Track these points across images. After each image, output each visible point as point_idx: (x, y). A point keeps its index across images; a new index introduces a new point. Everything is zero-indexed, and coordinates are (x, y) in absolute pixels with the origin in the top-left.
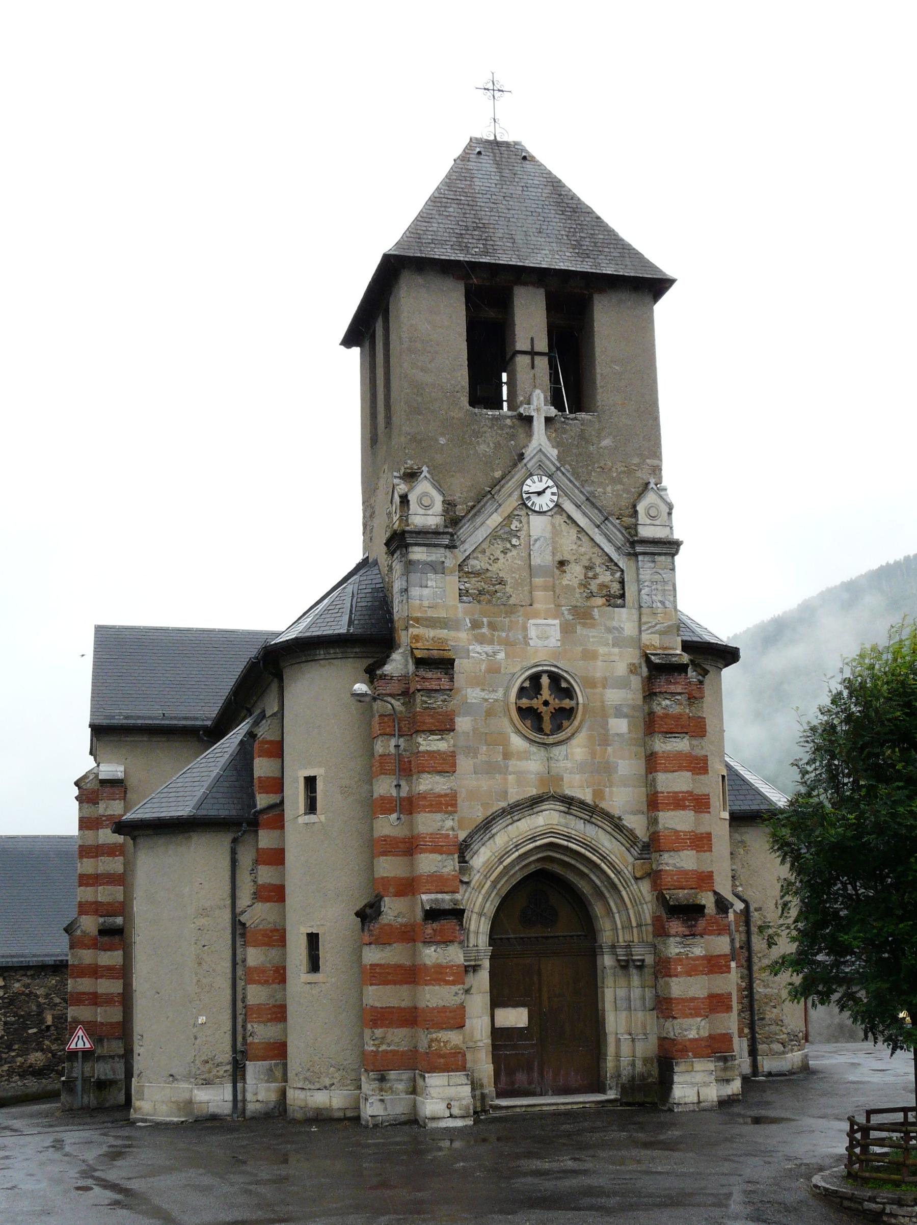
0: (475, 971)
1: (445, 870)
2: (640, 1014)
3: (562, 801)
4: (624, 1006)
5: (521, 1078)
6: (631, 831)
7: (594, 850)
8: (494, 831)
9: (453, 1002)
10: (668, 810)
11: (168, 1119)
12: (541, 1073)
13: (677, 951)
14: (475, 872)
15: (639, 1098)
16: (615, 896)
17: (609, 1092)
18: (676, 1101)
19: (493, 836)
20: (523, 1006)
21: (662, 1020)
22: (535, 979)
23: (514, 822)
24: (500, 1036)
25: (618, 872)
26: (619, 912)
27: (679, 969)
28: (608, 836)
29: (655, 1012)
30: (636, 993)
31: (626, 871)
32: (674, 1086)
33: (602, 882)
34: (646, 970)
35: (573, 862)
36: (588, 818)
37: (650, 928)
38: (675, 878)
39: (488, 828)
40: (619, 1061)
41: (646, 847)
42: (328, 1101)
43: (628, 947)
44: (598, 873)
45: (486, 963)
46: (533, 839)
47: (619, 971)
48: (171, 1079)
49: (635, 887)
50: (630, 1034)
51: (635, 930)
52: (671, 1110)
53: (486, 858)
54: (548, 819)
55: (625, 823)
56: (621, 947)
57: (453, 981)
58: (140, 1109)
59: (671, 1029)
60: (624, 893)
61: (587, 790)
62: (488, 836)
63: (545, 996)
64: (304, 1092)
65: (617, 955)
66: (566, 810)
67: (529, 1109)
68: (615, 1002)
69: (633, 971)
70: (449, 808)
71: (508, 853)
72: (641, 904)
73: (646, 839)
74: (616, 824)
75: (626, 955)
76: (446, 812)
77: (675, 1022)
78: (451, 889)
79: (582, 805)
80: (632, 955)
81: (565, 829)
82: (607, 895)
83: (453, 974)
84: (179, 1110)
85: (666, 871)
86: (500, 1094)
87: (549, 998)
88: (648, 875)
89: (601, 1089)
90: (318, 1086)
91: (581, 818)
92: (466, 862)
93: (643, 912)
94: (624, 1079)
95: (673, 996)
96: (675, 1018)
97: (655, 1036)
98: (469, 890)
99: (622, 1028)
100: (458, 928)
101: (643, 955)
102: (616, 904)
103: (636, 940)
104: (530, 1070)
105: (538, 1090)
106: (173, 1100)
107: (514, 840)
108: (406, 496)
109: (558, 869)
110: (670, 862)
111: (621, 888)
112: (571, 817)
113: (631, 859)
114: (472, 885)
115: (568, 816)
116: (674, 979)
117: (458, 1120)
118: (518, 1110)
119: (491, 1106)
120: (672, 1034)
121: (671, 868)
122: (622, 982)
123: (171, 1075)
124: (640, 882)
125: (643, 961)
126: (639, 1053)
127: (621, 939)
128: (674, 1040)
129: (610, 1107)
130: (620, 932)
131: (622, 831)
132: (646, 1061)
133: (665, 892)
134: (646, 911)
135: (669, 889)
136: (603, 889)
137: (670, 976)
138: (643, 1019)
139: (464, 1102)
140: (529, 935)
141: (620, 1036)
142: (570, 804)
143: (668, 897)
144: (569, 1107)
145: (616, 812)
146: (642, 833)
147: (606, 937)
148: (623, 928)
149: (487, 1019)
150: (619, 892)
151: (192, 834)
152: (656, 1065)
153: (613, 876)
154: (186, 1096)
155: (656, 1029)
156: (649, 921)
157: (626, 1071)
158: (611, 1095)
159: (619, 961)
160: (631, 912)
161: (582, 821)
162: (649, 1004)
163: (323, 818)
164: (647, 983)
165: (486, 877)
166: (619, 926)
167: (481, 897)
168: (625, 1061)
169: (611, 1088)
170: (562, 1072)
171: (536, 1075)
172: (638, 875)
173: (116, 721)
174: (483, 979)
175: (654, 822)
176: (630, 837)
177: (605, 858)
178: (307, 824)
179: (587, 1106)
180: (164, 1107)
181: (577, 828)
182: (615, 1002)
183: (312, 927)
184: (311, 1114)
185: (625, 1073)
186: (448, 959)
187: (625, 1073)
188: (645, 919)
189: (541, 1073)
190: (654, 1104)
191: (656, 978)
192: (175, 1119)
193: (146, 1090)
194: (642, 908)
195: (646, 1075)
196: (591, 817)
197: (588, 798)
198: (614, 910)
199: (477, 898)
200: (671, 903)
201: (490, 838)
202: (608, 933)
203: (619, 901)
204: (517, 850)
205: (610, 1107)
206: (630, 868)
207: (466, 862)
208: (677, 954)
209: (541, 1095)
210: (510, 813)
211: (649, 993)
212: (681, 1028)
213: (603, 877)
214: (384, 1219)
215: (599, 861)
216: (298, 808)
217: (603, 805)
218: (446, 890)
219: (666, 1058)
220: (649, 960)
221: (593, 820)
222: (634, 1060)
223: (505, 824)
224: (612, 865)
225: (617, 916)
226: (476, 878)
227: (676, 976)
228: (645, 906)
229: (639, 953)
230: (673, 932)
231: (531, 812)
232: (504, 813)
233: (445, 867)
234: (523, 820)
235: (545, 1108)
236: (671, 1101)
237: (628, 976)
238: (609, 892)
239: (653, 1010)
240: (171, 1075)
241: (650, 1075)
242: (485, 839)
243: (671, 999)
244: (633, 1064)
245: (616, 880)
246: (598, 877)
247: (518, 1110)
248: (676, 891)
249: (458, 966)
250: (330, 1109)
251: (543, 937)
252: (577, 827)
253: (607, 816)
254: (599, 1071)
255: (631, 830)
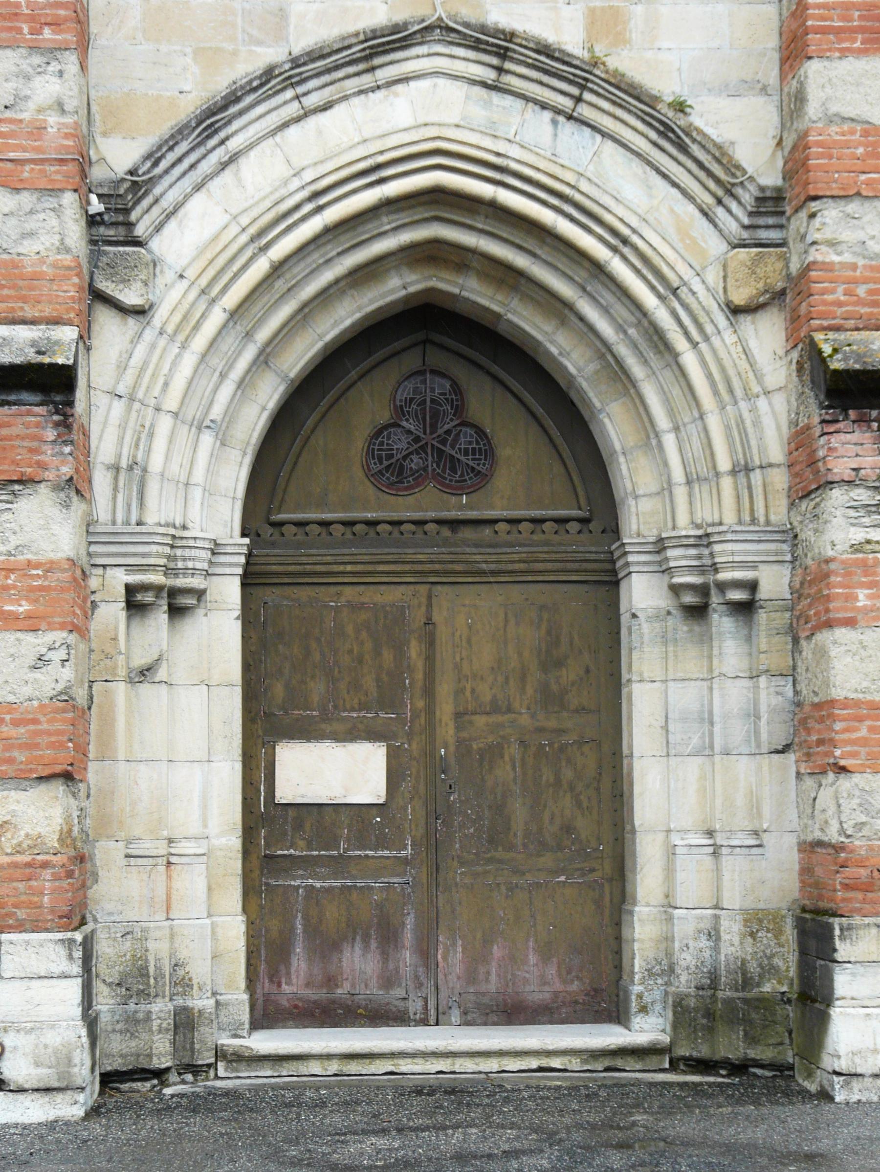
0: (176, 611)
1: (29, 247)
2: (744, 769)
3: (476, 45)
4: (695, 740)
5: (359, 966)
6: (721, 154)
7: (588, 215)
8: (234, 144)
9: (27, 691)
10: (844, 53)
12: (426, 953)
13: (858, 535)
14: (170, 276)
15: (731, 1045)
16: (667, 376)
17: (638, 1021)
18: (843, 1065)
19: (233, 158)
20: (372, 736)
21: (809, 782)
22: (414, 651)
23: (307, 114)
24: (274, 833)
25: (671, 291)
26: (676, 429)
27: (863, 598)
28: (637, 166)
29: (791, 758)
30: (732, 696)
31: (697, 286)
32: (836, 1012)
33: (621, 329)
34: (762, 616)
35: (520, 261)
36: (566, 103)
37: (780, 479)
38: (861, 291)
39: (212, 131)
40: (670, 919)
41: (771, 205)
43: (704, 540)
44: (607, 297)
45: (228, 591)
46: (374, 172)
47: (679, 626)
49: (729, 337)
50: (710, 833)
51: (727, 483)
52: (825, 1096)
53: (208, 233)
54: (430, 107)
55: (697, 120)
56: (682, 543)
57: (29, 617)
59: (832, 810)
60: (689, 360)
61: (567, 12)
62: (214, 158)
63: (445, 710)
65: (668, 571)
66: (490, 75)
67: (354, 1067)
68: (666, 728)
69: (722, 623)
70: (47, 33)
71: (286, 218)
72: (749, 396)
73: (771, 179)
74: (669, 130)
75: (701, 570)
76: (34, 48)
77: (845, 783)
78: (48, 311)
79: (548, 59)
80: (715, 568)
81: (488, 143)
82: (637, 370)
83: (32, 593)
85: (828, 267)
86: (265, 1016)
87: (458, 715)
88: (775, 298)
89: (616, 1012)
91: (544, 106)
92: (137, 243)
93: (757, 423)
94: (684, 982)
95: (838, 693)
96: (843, 769)
97: (791, 840)
98: (149, 335)
99: (686, 814)
100: (51, 434)
101: (753, 566)
102: (667, 401)
103: (730, 518)
104: (388, 936)
105: (415, 1006)
107: (308, 176)
109: (475, 292)
110: (847, 235)
111: (680, 343)
112: (508, 100)
113: (716, 246)
114: (159, 317)
115: (496, 98)
116: (841, 633)
117: (25, 1100)
118: (315, 1067)
119: (220, 1054)
120: (834, 826)
121: (847, 258)
122: (690, 661)
124: (746, 323)
125: (752, 586)
126: (733, 898)
127: (683, 519)
128: (838, 848)
129: (633, 1072)
130: (681, 493)
131: (683, 148)
132: (756, 922)
133: (819, 337)
134: (768, 422)
135: (837, 329)
136: (623, 351)
137: (829, 624)
138: (757, 785)
139: (54, 1039)
140: (395, 516)
141: (676, 839)
142: (503, 54)
143: (827, 349)
144: (492, 1065)
145: (665, 85)
146: (761, 165)
147: (640, 518)
148: (689, 482)
149: (227, 775)
150: (676, 355)
152: (790, 933)
153: (649, 300)
155: (792, 814)
156: (776, 452)
157: (690, 958)
158: (647, 1029)
159: (676, 590)
160: (714, 423)
161: (547, 115)
162: (773, 731)
164: (765, 661)
165: (208, 295)
166: (678, 475)
167: (189, 361)
168: (686, 924)
169: (644, 1009)
170: (497, 951)
171: (407, 957)
172: (739, 297)
174: (218, 634)
175: (794, 104)
176: (720, 175)
177: (625, 241)
179: (556, 1063)
181: (527, 137)
182: (666, 728)
185: (686, 959)
186: (14, 541)
187: (686, 959)
188: (762, 449)
189: (426, 953)
190: (782, 1069)
191: (796, 641)
194: (753, 410)
195: (753, 967)
196: (579, 100)
197: (570, 38)
198: (663, 422)
199: (174, 364)
200: (836, 364)
201: (224, 166)
202: (645, 505)
203: (676, 392)
204: (320, 209)
205: (633, 1072)
206: (713, 276)
207: (137, 243)
208: (856, 548)
209: (424, 1022)
210: (290, 82)
211: (772, 696)
212: (864, 807)
213: (622, 312)
215: (600, 252)
217: (624, 62)
218: (30, 312)
219: (817, 912)
220: (774, 583)
221: (584, 111)
222: (717, 917)
223: (274, 120)
224: (648, 267)
225: (669, 441)
226: (170, 299)
227: (850, 623)
228: (762, 404)
229: (735, 559)
230: (841, 468)
231: (366, 80)
232: (267, 82)
233: (31, 234)
234: (339, 110)
235: (405, 1066)
236: (828, 1062)
237: (706, 639)
238: (645, 362)
239: (784, 750)
241: (769, 970)
242: (206, 167)
243: (832, 703)
244: (714, 935)
245: (662, 317)
246: (606, 310)
247: (315, 1067)
248: (865, 334)
249: (50, 567)
251: (439, 522)
252: (526, 135)
253: (631, 96)
254: (618, 952)
255: (719, 147)
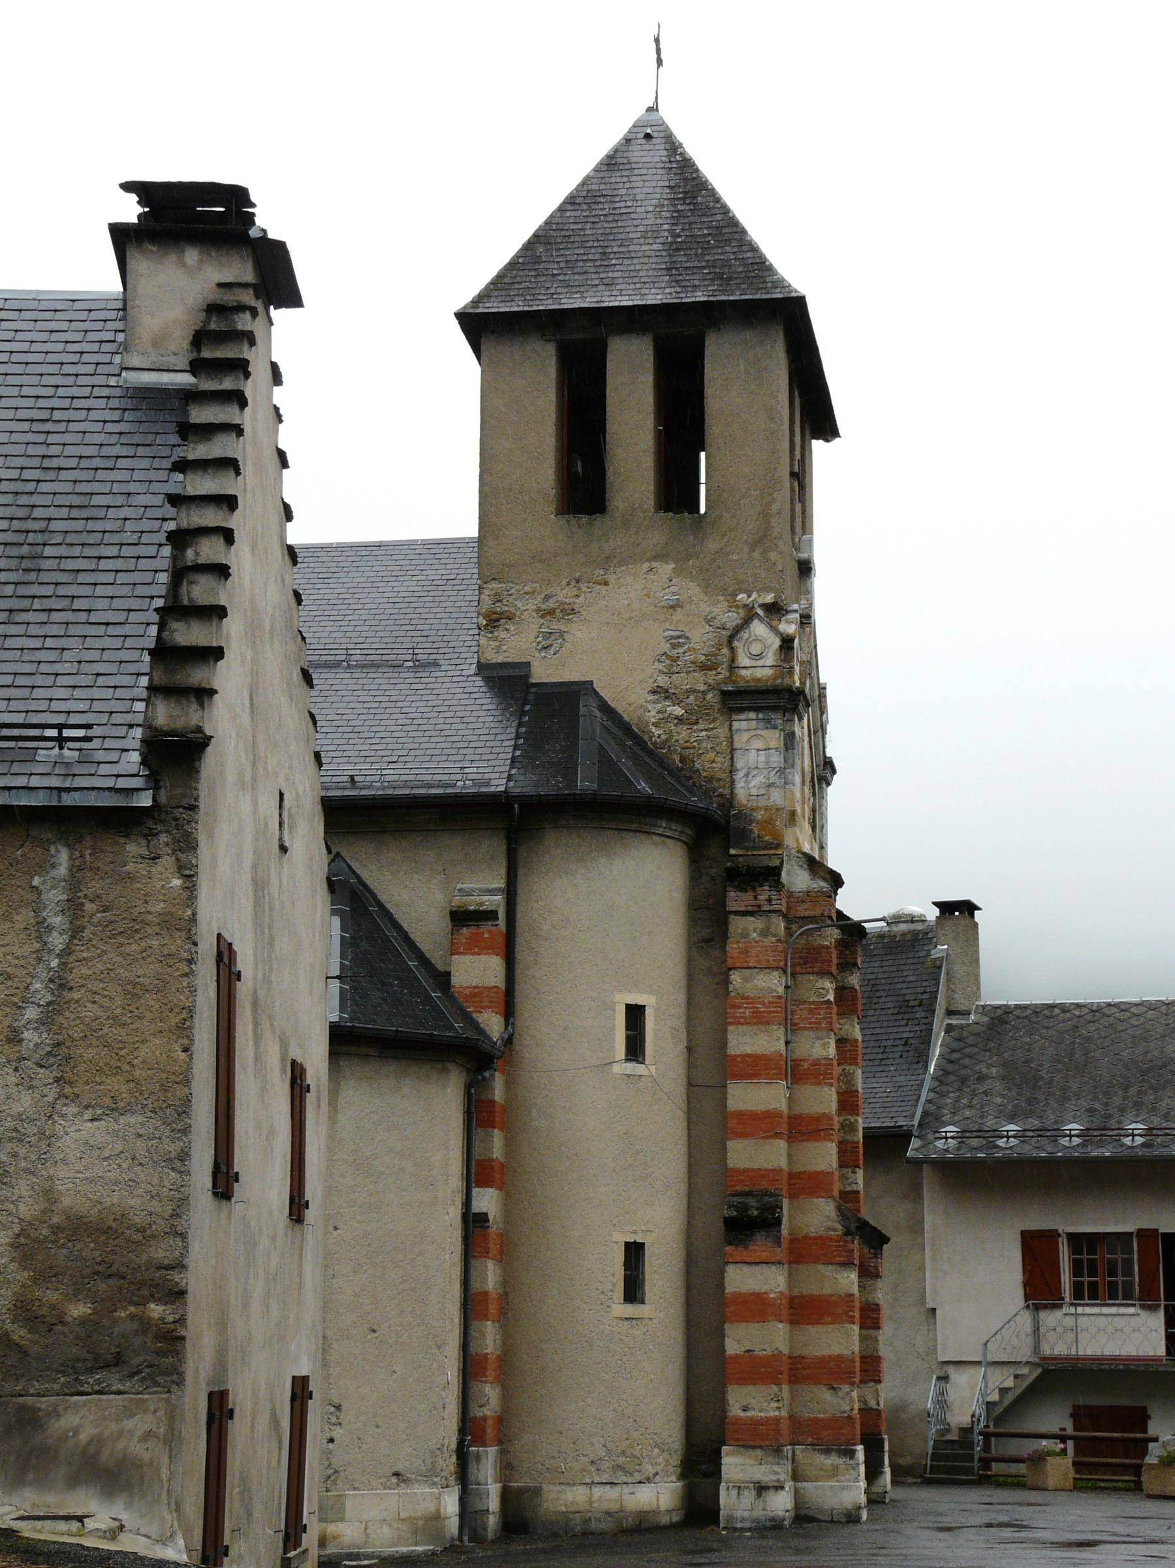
11: (405, 1549)
42: (654, 1500)
48: (394, 1480)
58: (335, 1538)
64: (618, 1489)
84: (415, 1532)
90: (638, 1477)
106: (403, 1515)
108: (792, 640)
123: (396, 1474)
151: (450, 1066)
154: (431, 1507)
163: (653, 1069)
173: (493, 789)
178: (629, 1076)
180: (386, 1530)
183: (634, 1232)
184: (629, 1522)
192: (420, 1549)
193: (349, 1504)
214: (71, 1565)
216: (613, 1049)
240: (396, 1474)
250: (656, 1512)
